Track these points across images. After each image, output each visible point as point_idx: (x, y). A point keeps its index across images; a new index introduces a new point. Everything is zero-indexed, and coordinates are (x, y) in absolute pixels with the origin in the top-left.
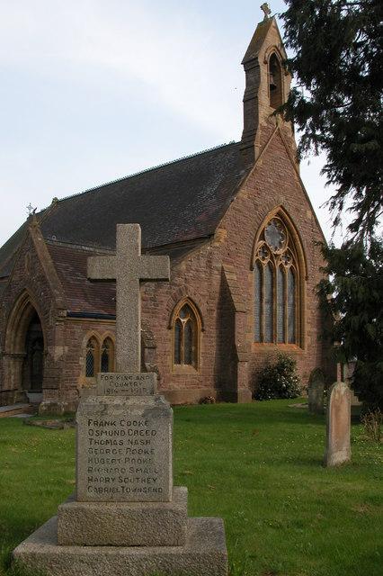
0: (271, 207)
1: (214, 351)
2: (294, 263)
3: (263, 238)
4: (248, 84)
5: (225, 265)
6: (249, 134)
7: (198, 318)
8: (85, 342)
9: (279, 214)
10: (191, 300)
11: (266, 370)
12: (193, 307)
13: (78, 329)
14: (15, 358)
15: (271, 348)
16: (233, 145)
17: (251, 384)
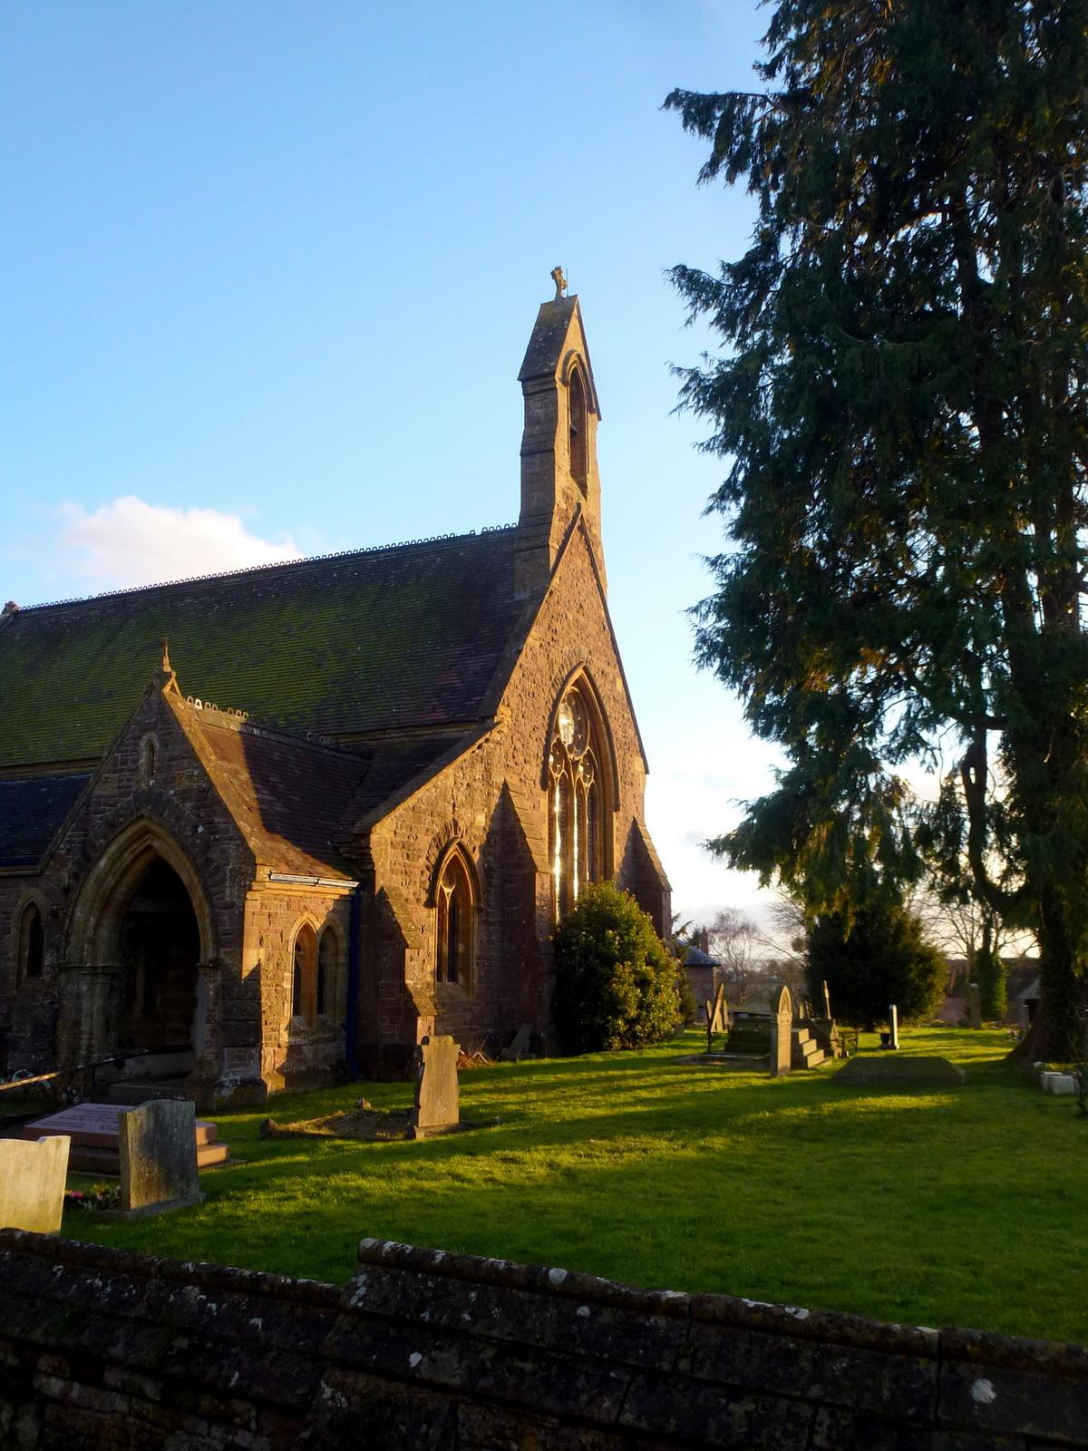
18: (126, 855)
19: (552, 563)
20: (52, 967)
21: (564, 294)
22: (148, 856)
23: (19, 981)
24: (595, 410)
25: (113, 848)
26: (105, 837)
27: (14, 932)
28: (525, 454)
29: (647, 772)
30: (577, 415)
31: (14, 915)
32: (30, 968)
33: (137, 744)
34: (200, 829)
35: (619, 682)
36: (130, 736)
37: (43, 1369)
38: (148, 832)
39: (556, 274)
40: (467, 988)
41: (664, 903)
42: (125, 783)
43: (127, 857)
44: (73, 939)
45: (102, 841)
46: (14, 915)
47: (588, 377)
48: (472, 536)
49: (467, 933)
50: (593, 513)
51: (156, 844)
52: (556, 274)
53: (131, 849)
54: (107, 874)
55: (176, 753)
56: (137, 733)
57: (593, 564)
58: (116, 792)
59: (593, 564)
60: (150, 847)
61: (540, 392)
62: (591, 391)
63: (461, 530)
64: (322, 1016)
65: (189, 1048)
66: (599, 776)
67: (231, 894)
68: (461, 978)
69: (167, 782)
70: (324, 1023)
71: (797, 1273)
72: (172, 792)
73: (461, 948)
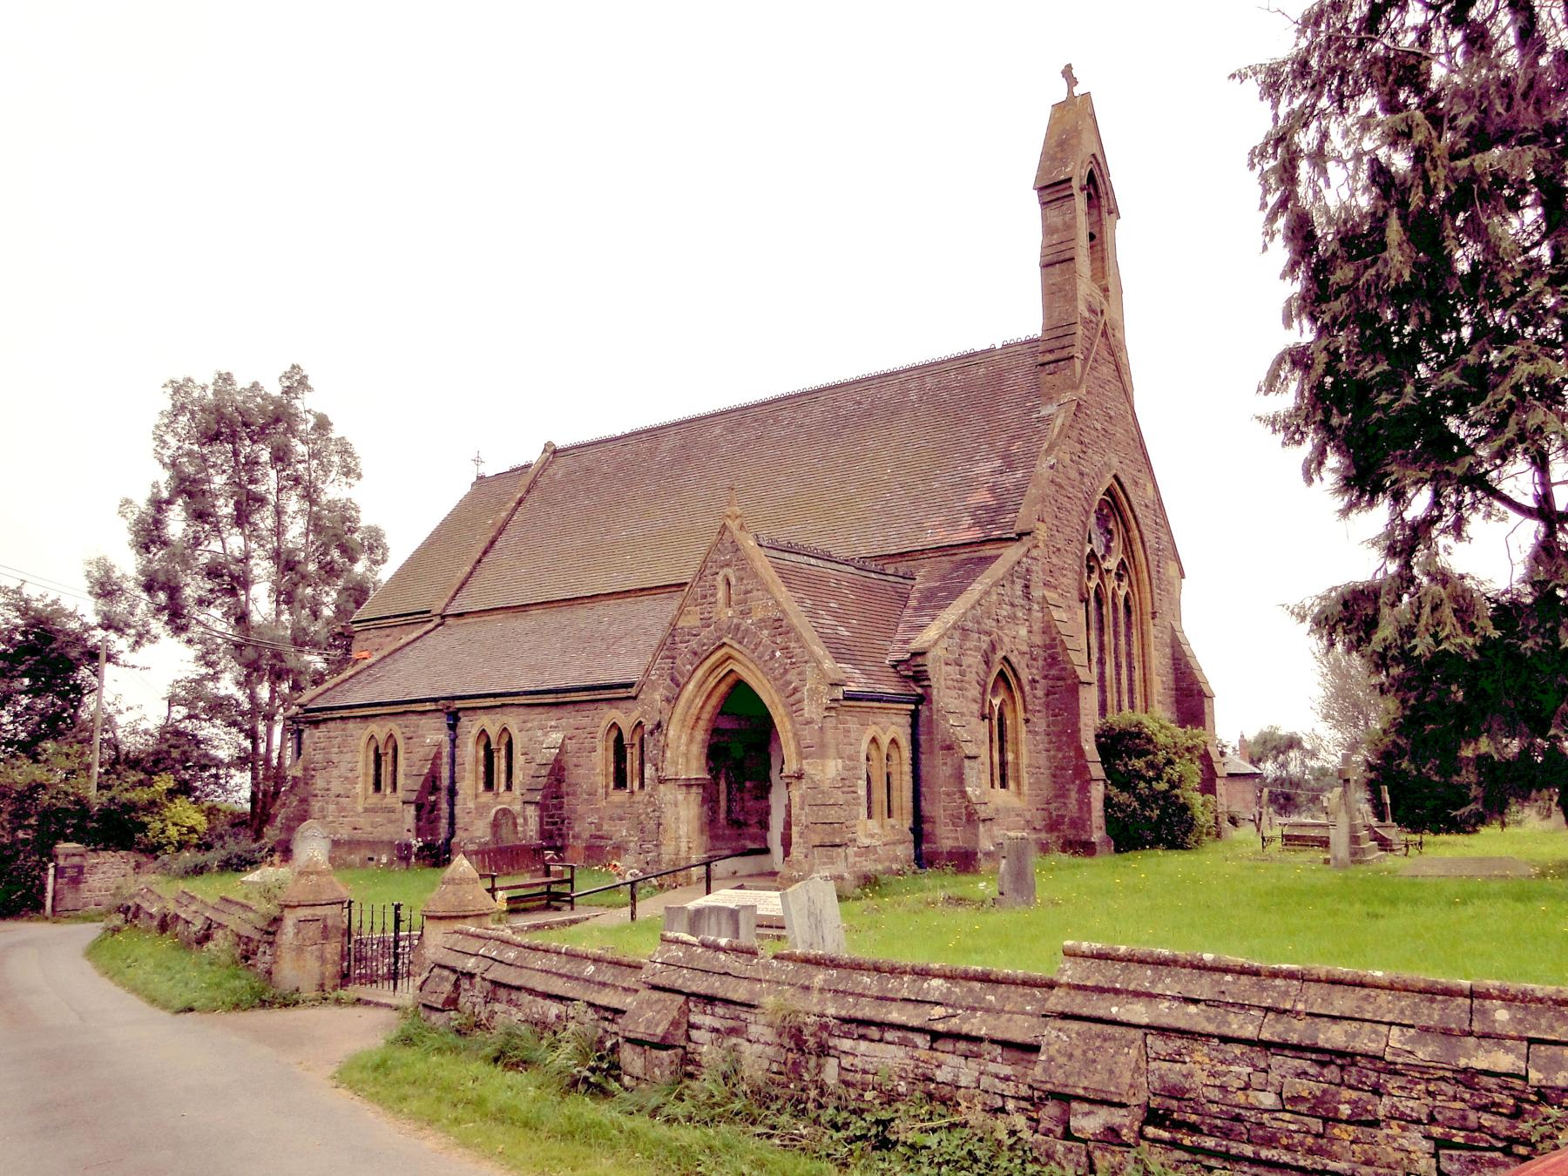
0: (1100, 475)
1: (1042, 760)
2: (1131, 585)
3: (1090, 541)
4: (1048, 230)
5: (1047, 594)
6: (1060, 332)
7: (1017, 695)
8: (864, 745)
9: (1109, 492)
10: (1010, 664)
11: (1507, 592)
12: (1010, 674)
13: (852, 723)
14: (689, 786)
15: (668, 1133)
16: (1030, 342)
17: (129, 800)
18: (711, 679)
19: (1078, 375)
20: (652, 779)
21: (1077, 91)
22: (730, 680)
23: (607, 794)
24: (1114, 211)
25: (700, 673)
26: (691, 664)
27: (600, 750)
28: (1046, 266)
29: (1183, 576)
30: (1095, 218)
31: (599, 735)
32: (616, 780)
33: (715, 580)
34: (778, 654)
35: (1150, 487)
36: (707, 572)
37: (1344, 1118)
38: (730, 658)
39: (1067, 73)
40: (1019, 793)
41: (1207, 710)
42: (706, 615)
43: (712, 682)
44: (668, 754)
45: (689, 667)
46: (599, 735)
47: (1105, 174)
48: (991, 350)
49: (1016, 742)
50: (1115, 316)
51: (737, 668)
52: (1067, 73)
53: (716, 673)
54: (695, 697)
55: (750, 587)
56: (714, 570)
57: (1118, 369)
58: (698, 623)
59: (1118, 369)
60: (731, 671)
61: (1058, 199)
62: (1110, 192)
63: (979, 343)
64: (892, 821)
65: (766, 851)
66: (1134, 583)
67: (809, 711)
68: (1012, 784)
69: (745, 614)
70: (893, 827)
71: (1185, 1063)
72: (749, 621)
73: (1010, 757)
